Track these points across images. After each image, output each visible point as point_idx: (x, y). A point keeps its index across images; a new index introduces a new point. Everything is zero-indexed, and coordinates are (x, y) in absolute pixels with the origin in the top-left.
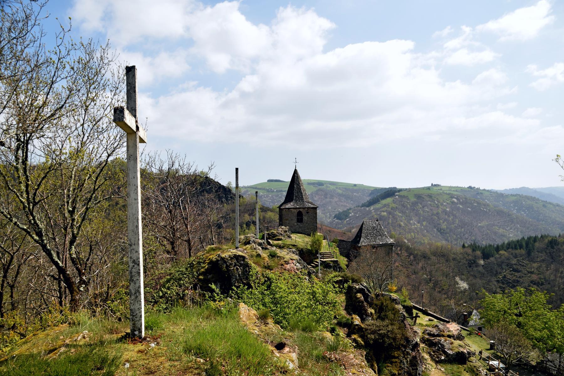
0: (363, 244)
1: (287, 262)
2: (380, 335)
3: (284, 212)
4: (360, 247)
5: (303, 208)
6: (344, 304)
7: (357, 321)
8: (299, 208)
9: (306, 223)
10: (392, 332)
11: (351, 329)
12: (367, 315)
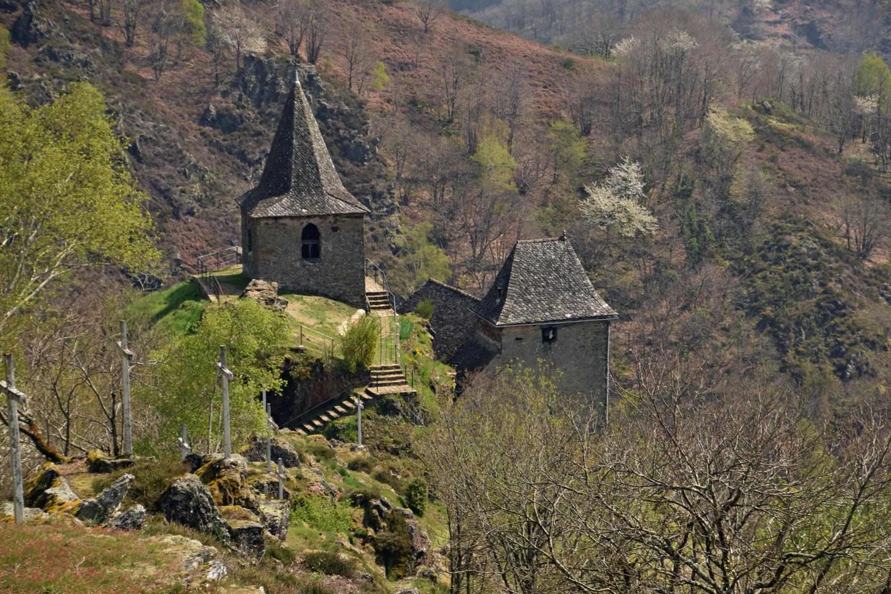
0: (511, 320)
1: (312, 485)
2: (389, 543)
3: (261, 229)
4: (501, 329)
5: (321, 217)
6: (362, 519)
7: (371, 532)
8: (309, 217)
9: (332, 262)
10: (398, 541)
11: (365, 539)
12: (380, 528)
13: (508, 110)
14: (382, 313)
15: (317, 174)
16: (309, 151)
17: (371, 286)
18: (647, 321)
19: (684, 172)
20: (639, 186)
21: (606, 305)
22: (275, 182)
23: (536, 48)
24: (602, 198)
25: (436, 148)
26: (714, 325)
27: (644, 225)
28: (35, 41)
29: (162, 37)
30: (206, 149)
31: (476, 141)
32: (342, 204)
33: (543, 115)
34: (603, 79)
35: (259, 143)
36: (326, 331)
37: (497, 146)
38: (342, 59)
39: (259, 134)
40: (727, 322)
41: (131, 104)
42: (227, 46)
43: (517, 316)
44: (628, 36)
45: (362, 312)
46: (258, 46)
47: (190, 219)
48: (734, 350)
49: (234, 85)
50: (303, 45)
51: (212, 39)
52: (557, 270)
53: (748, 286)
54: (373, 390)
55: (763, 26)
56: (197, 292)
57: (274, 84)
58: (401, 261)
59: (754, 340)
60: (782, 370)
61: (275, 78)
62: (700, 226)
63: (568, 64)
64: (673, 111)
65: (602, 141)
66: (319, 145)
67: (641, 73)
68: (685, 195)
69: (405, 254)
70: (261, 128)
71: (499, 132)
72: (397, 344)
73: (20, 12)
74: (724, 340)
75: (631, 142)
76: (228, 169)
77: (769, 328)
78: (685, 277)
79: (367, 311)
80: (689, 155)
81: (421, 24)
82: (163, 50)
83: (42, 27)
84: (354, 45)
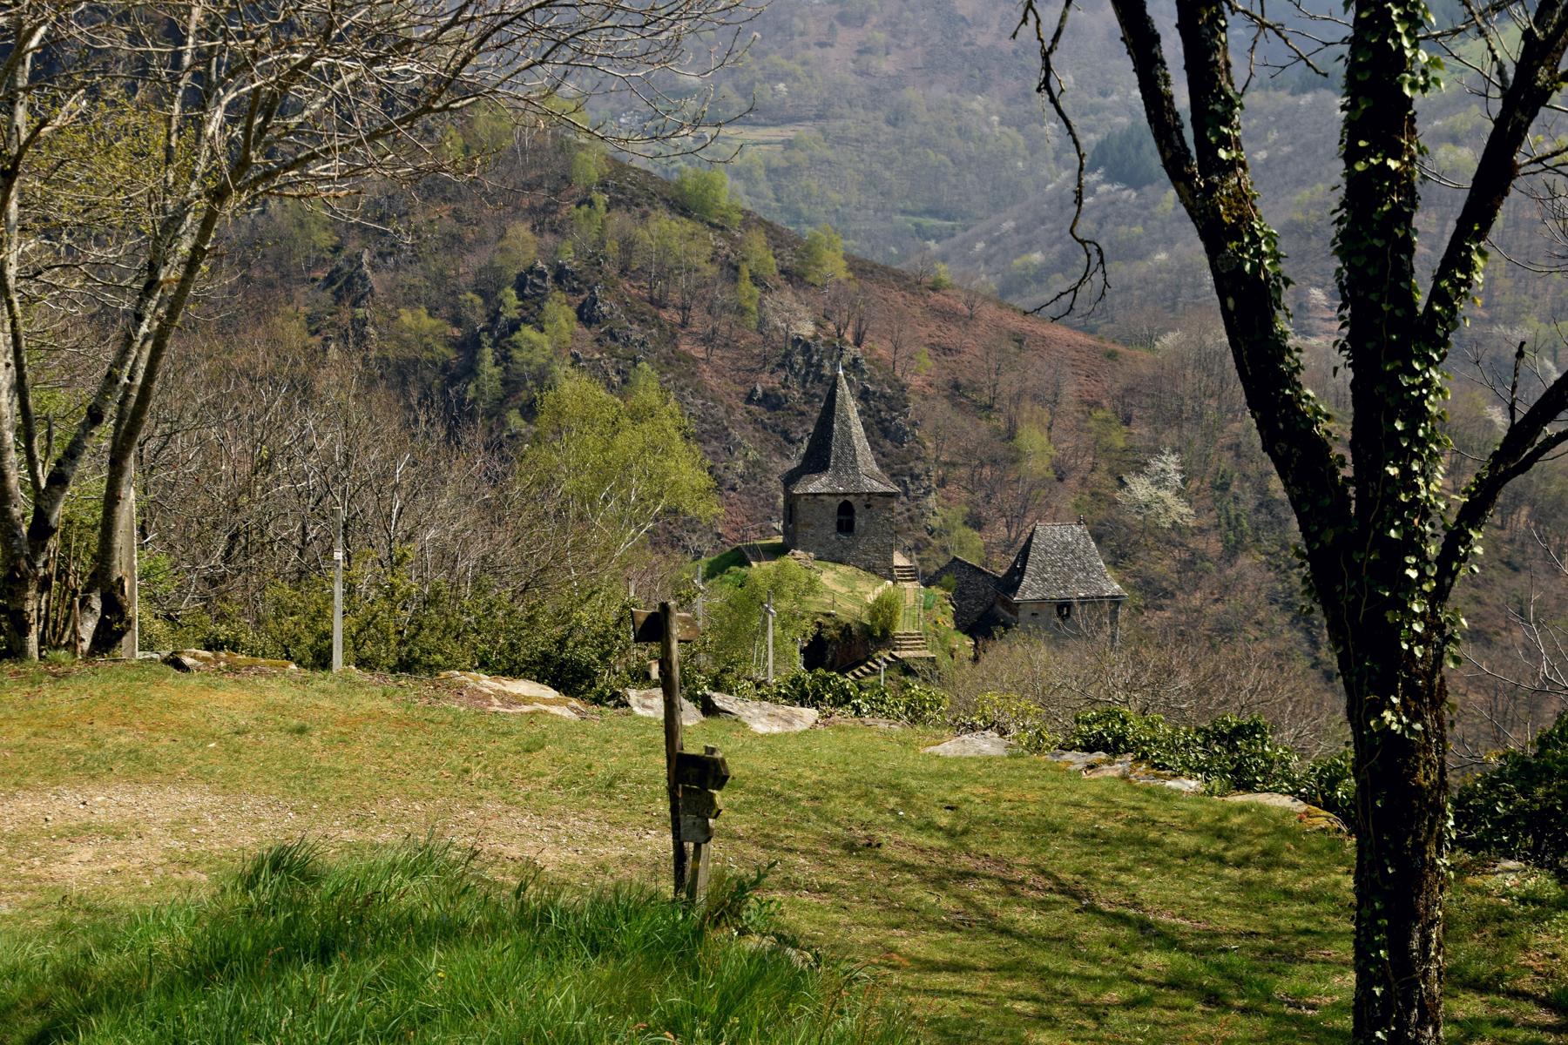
0: (1028, 596)
3: (801, 505)
13: (1051, 398)
14: (906, 585)
15: (854, 456)
16: (848, 436)
17: (899, 560)
18: (1180, 612)
19: (1223, 466)
20: (1178, 477)
21: (1117, 586)
22: (817, 460)
23: (1081, 338)
24: (1141, 488)
25: (977, 431)
26: (1248, 618)
27: (1181, 516)
28: (598, 322)
29: (715, 319)
30: (750, 427)
31: (1015, 427)
32: (875, 484)
33: (1084, 402)
34: (1146, 370)
35: (802, 423)
36: (856, 599)
37: (1037, 433)
38: (886, 343)
39: (802, 414)
40: (1261, 615)
41: (682, 382)
42: (776, 329)
43: (1034, 593)
44: (1173, 330)
45: (890, 583)
46: (807, 329)
47: (733, 494)
48: (1267, 644)
49: (781, 366)
50: (850, 329)
51: (762, 322)
52: (1073, 552)
53: (1283, 581)
54: (896, 654)
55: (1318, 322)
56: (740, 558)
57: (820, 365)
58: (936, 542)
59: (1287, 636)
60: (1313, 666)
61: (821, 360)
62: (1237, 517)
63: (1112, 355)
64: (1215, 404)
65: (1141, 431)
66: (858, 430)
67: (1184, 367)
68: (1224, 487)
69: (940, 535)
70: (805, 408)
71: (1039, 420)
72: (919, 612)
73: (586, 294)
74: (1257, 634)
75: (1170, 436)
76: (771, 447)
77: (1302, 624)
78: (1220, 571)
79: (895, 582)
80: (1230, 448)
81: (966, 311)
82: (714, 331)
83: (605, 309)
84: (900, 331)
